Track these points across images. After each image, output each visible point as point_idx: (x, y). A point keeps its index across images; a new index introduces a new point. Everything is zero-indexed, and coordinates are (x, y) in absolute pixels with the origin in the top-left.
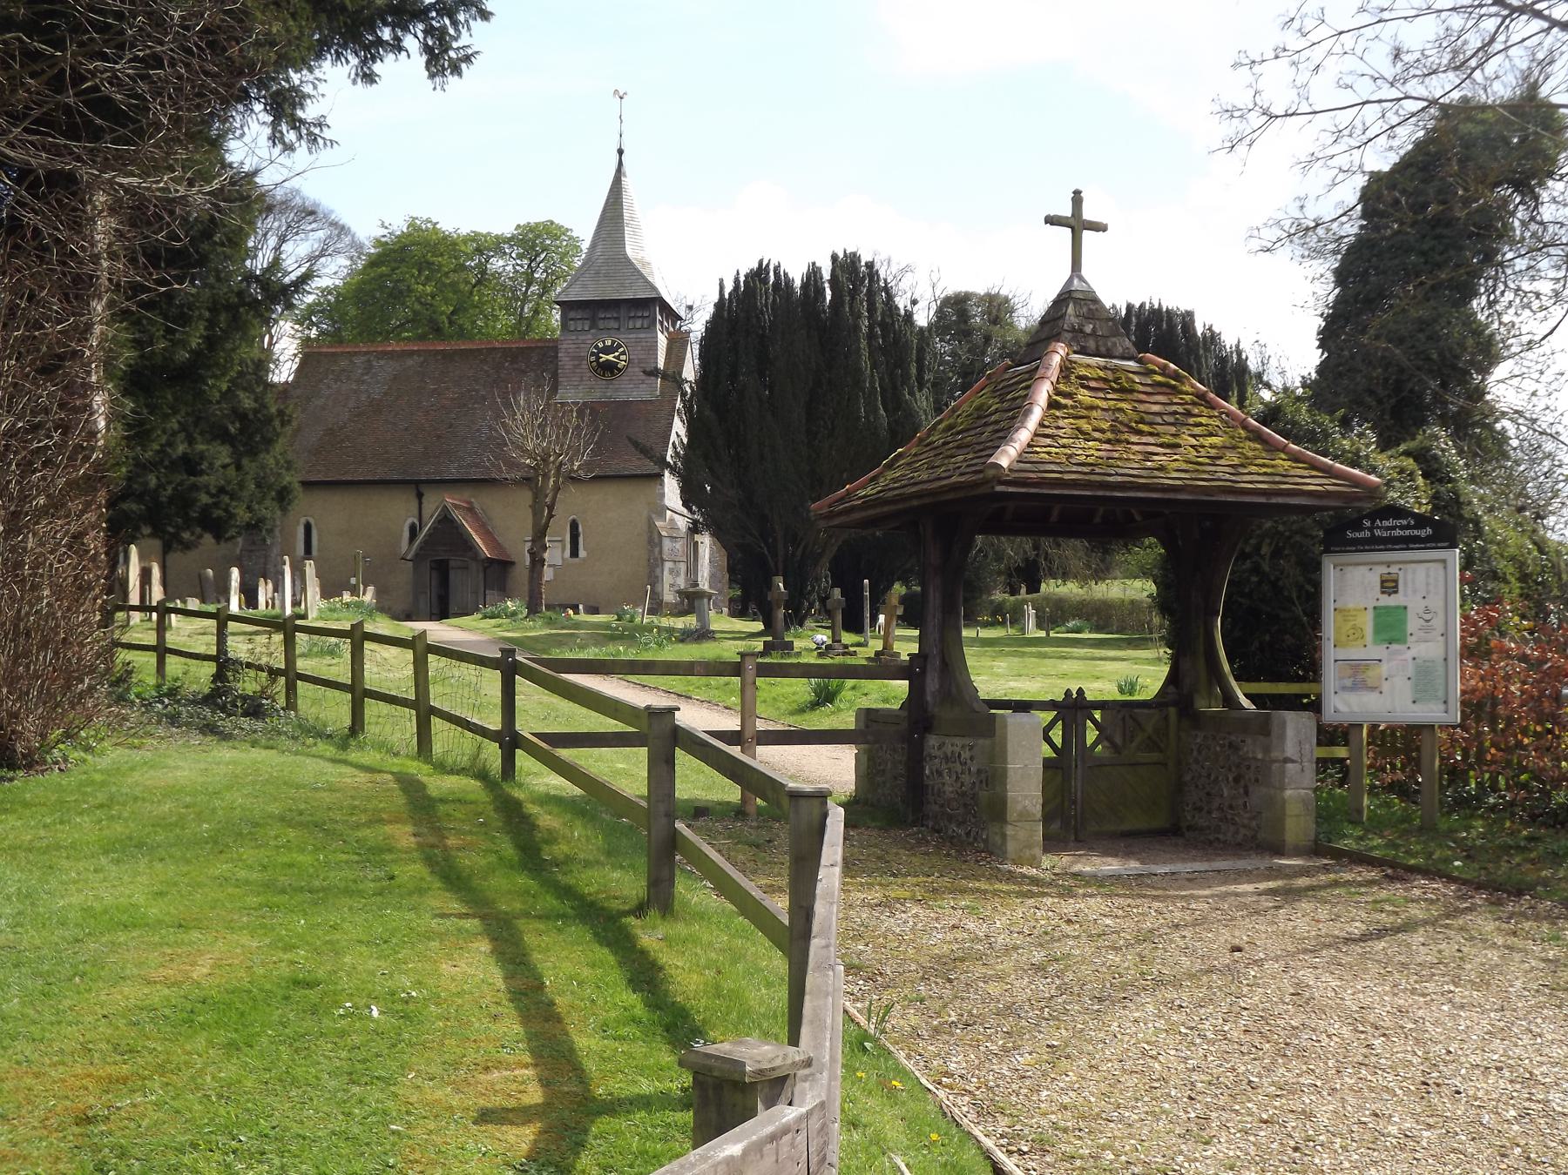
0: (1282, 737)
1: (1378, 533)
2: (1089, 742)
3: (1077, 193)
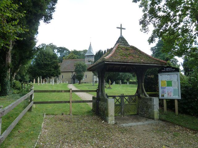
0: (153, 101)
1: (167, 70)
2: (125, 101)
3: (121, 24)
